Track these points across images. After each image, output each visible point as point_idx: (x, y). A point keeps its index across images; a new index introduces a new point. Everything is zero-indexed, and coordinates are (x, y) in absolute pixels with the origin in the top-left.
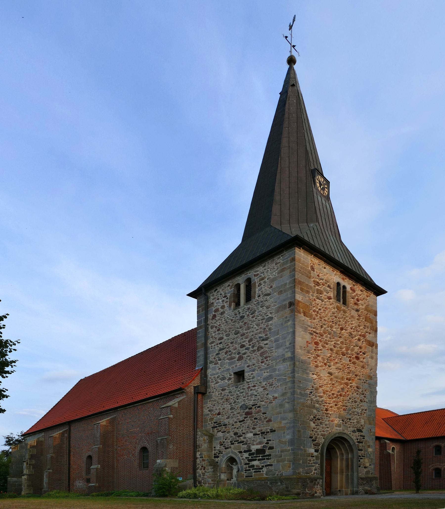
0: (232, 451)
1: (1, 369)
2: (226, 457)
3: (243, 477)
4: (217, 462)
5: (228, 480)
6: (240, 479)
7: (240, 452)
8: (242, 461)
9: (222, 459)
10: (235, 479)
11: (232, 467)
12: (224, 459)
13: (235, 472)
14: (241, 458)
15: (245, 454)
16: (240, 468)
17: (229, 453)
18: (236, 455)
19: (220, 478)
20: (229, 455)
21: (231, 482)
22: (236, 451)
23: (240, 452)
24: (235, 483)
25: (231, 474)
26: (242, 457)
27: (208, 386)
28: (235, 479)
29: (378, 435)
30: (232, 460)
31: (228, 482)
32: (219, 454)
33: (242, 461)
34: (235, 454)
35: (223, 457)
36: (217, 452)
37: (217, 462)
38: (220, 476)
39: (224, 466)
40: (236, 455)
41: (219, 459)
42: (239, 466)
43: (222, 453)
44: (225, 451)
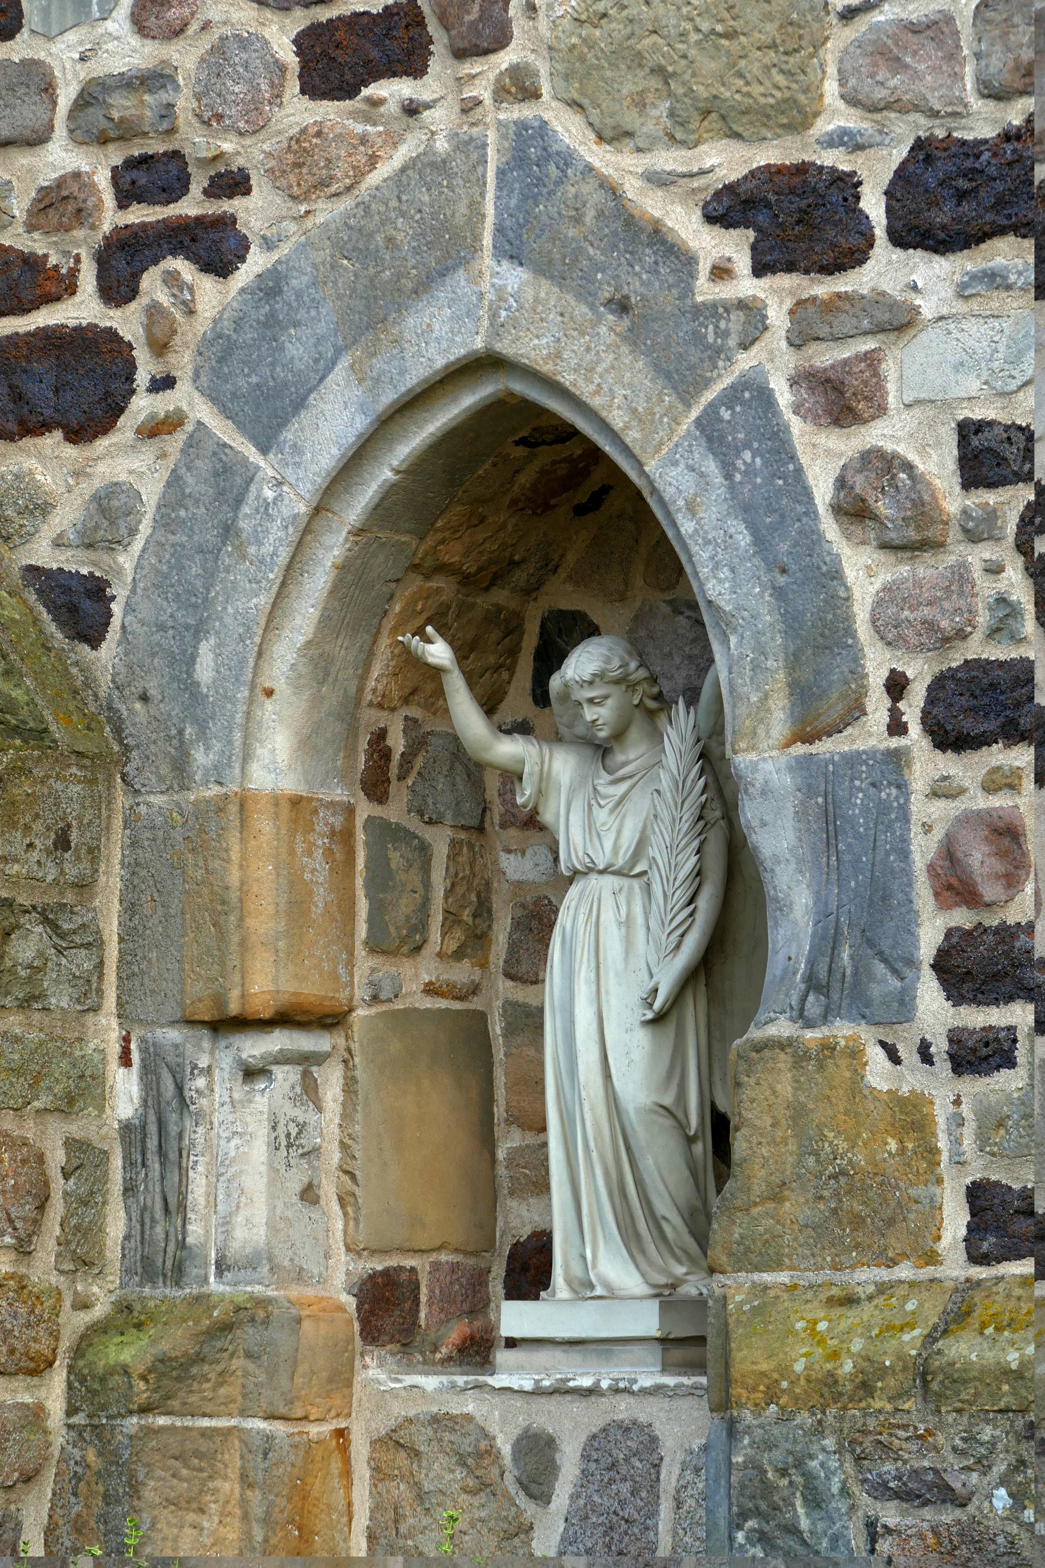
0: (533, 157)
1: (5, 859)
2: (334, 420)
3: (869, 1215)
4: (80, 607)
5: (385, 1308)
6: (808, 1319)
7: (796, 220)
8: (864, 574)
9: (230, 482)
10: (606, 1288)
11: (492, 812)
12: (286, 481)
13: (605, 984)
14: (822, 458)
15: (928, 279)
16: (777, 837)
17: (447, 251)
18: (681, 342)
19: (163, 1259)
20: (436, 334)
21: (499, 1402)
22: (666, 181)
23: (796, 220)
24: (623, 1456)
25: (482, 1064)
26: (841, 399)
27: (329, 479)
28: (606, 1288)
29: (888, 1064)
30: (529, 533)
31: (394, 1388)
32: (122, 265)
33: (864, 574)
34: (614, 258)
35: (270, 413)
36: (60, 204)
37: (80, 607)
38: (160, 1140)
39: (276, 756)
40: (681, 342)
41: (122, 460)
42: (766, 762)
43: (215, 247)
44: (305, 169)
